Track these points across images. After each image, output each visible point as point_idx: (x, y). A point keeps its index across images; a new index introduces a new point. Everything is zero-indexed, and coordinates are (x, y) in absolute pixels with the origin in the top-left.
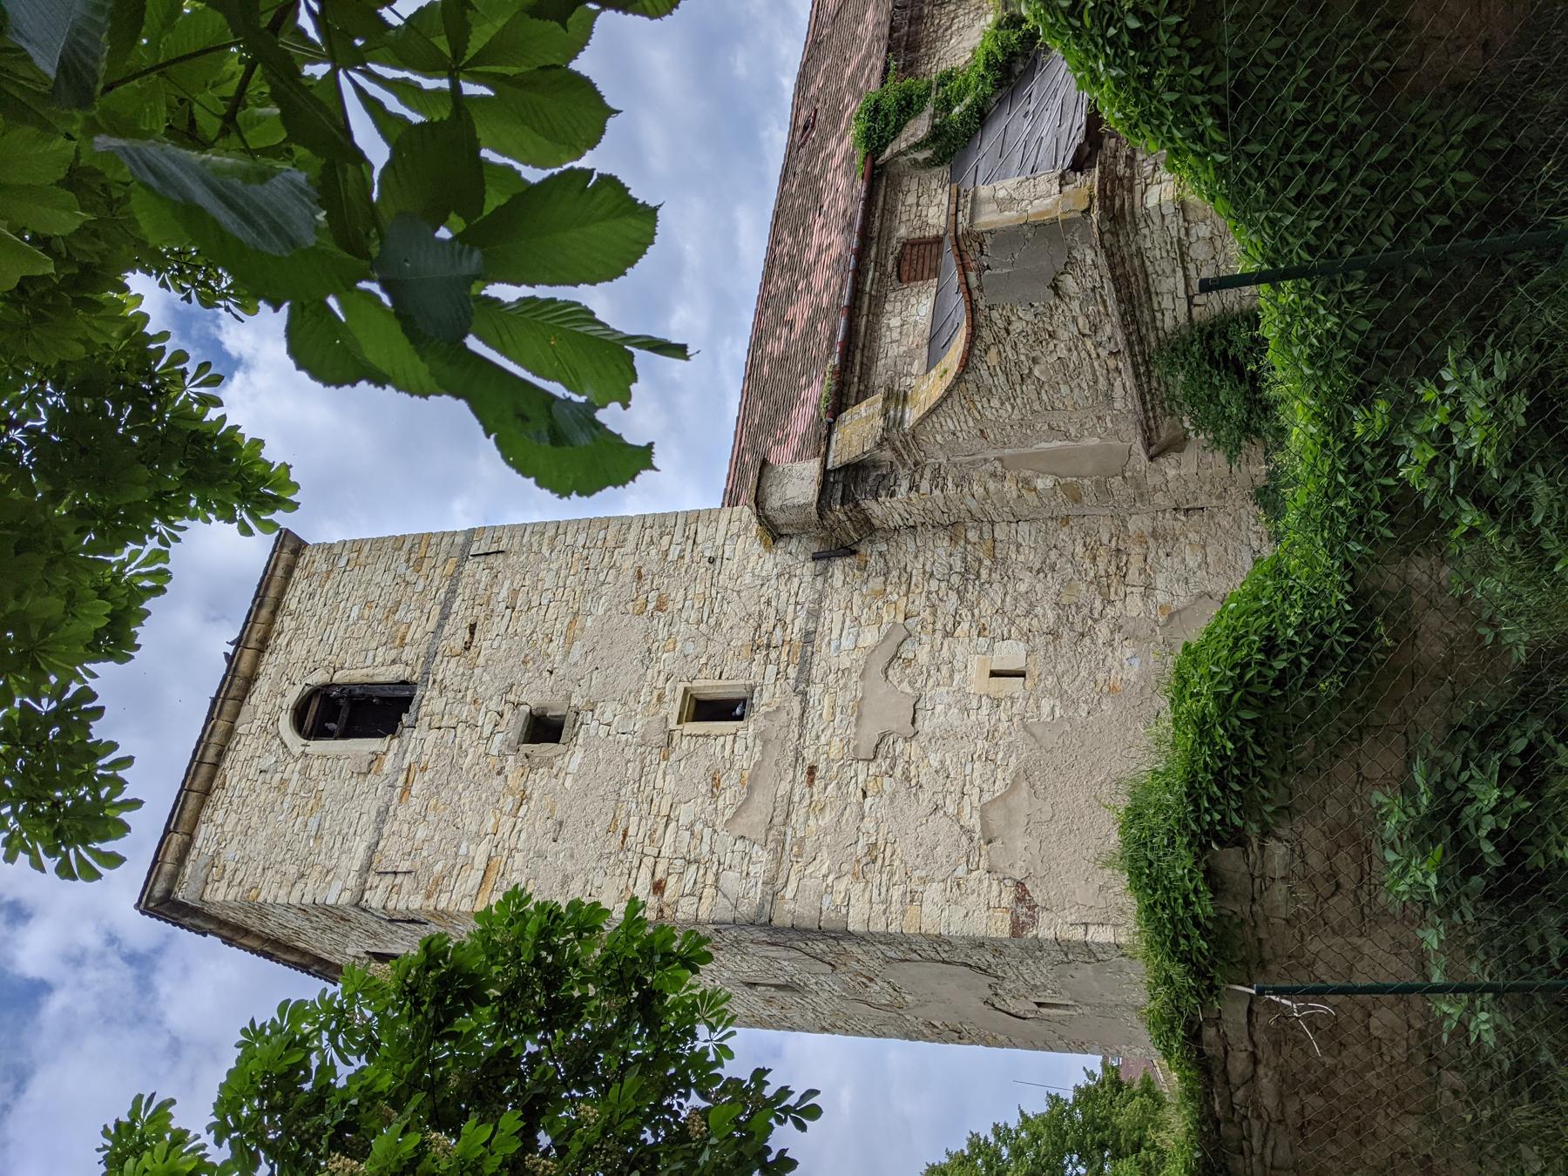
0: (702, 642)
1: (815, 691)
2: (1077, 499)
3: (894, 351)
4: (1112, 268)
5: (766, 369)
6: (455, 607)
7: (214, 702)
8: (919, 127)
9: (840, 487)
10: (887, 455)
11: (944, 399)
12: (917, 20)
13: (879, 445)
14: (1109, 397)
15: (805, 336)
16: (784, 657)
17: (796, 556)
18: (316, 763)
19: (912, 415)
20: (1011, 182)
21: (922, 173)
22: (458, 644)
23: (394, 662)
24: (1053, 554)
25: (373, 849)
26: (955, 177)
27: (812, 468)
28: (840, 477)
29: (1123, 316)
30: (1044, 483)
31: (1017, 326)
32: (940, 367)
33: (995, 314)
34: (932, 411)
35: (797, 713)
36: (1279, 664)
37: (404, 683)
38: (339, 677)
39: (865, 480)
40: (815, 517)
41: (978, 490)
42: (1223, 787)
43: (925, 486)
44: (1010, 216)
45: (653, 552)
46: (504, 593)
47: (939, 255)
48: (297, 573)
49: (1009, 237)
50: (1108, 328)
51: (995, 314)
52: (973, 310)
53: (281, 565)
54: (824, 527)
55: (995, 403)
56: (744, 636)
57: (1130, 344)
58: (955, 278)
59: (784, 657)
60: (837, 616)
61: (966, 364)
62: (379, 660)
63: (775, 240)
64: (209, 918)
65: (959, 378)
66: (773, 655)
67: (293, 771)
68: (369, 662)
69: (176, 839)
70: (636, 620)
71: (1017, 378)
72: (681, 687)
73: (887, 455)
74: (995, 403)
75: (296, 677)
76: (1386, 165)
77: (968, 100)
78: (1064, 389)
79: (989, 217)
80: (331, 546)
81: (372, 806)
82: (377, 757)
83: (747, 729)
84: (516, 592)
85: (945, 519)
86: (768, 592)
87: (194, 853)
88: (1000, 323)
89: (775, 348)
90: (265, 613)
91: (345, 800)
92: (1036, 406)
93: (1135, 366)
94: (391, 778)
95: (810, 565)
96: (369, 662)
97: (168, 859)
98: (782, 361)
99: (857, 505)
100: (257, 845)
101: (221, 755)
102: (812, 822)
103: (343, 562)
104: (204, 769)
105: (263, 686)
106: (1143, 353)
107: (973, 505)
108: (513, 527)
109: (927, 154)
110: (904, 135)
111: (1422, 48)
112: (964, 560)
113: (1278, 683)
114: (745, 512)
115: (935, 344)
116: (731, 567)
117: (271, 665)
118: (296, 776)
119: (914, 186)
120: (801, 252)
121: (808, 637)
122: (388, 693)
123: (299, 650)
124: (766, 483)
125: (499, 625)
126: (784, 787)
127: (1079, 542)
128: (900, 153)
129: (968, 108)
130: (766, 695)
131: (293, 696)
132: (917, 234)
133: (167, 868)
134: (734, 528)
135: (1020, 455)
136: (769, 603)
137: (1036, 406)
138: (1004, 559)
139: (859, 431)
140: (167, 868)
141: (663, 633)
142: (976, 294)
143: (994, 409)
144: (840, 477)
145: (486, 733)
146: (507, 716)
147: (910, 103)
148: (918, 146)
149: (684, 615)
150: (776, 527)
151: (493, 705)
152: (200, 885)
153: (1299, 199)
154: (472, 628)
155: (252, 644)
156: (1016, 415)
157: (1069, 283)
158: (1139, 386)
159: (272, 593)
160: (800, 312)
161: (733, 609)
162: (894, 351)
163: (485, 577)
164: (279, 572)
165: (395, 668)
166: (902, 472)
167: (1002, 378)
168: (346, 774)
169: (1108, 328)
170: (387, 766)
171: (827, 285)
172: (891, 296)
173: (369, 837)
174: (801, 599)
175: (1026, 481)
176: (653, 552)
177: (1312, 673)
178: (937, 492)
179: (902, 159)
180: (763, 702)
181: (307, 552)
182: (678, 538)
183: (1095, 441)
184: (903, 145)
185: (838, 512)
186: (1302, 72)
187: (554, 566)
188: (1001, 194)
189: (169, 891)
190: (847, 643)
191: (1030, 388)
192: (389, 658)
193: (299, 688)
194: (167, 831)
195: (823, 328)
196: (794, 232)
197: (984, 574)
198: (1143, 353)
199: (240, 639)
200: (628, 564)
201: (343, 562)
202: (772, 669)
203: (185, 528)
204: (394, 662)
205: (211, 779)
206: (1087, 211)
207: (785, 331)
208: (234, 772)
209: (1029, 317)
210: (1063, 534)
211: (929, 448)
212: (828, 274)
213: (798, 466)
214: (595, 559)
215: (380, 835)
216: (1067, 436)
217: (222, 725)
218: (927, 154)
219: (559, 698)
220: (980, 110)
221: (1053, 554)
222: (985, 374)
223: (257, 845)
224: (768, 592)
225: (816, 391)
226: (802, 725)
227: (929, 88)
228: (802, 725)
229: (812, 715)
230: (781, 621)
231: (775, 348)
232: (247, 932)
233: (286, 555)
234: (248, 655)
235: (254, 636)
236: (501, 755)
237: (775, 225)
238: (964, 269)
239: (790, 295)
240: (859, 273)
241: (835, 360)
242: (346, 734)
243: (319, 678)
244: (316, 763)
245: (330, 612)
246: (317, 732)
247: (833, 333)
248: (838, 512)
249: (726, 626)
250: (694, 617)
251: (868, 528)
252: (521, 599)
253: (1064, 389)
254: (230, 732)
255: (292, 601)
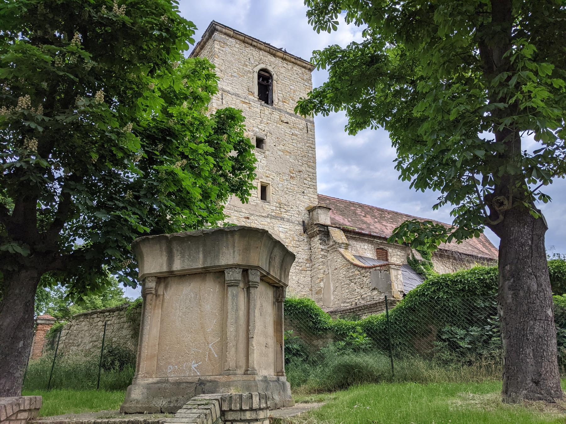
0: (282, 189)
1: (268, 220)
2: (317, 293)
3: (358, 246)
4: (379, 303)
5: (353, 208)
6: (293, 118)
7: (269, 45)
8: (418, 257)
9: (323, 230)
10: (331, 243)
11: (346, 259)
12: (448, 257)
13: (334, 241)
14: (344, 302)
15: (362, 221)
16: (277, 212)
17: (305, 217)
18: (251, 75)
19: (342, 250)
20: (402, 279)
21: (406, 257)
22: (283, 119)
23: (278, 99)
24: (302, 286)
25: (228, 92)
26: (404, 266)
27: (328, 222)
28: (326, 230)
29: (367, 306)
30: (322, 284)
31: (365, 279)
32: (354, 259)
33: (368, 273)
34: (343, 256)
35: (263, 215)
36: (314, 316)
37: (273, 102)
38: (274, 82)
39: (324, 237)
40: (315, 223)
41: (321, 267)
42: (289, 306)
43: (322, 253)
44: (393, 278)
45: (306, 176)
46: (296, 132)
47: (383, 260)
48: (304, 69)
49: (388, 277)
50: (363, 302)
51: (368, 273)
52: (370, 268)
53: (306, 65)
54: (311, 225)
55: (344, 273)
56: (283, 201)
57: (359, 307)
58: (377, 263)
59: (277, 212)
60: (288, 227)
61: (355, 265)
62: (279, 95)
63: (389, 212)
64: (207, 40)
65: (352, 263)
66: (278, 209)
67: (249, 68)
68: (279, 92)
69: (232, 33)
70: (288, 170)
71: (351, 278)
72: (270, 182)
73: (331, 243)
74: (344, 273)
75: (275, 69)
76: (401, 331)
77: (424, 270)
78: (347, 291)
79: (393, 273)
80: (311, 80)
81: (240, 92)
82: (253, 94)
83: (259, 201)
84: (297, 136)
85: (312, 258)
86: (295, 208)
87: (227, 38)
88: (366, 275)
89: (359, 211)
90: (293, 60)
91: (241, 84)
92: (343, 283)
93: (353, 309)
94: (247, 98)
95: (302, 220)
96: (279, 92)
97: (226, 30)
98: (355, 213)
99: (318, 234)
100: (229, 58)
101: (254, 46)
102: (235, 218)
103: (306, 84)
104: (250, 42)
105: (273, 59)
106: (356, 311)
107: (316, 266)
108: (314, 135)
109: (411, 258)
110: (416, 252)
111: (419, 340)
112: (302, 262)
113: (310, 316)
114: (316, 203)
115: (360, 257)
116: (302, 198)
117: (278, 61)
118: (248, 69)
119: (402, 254)
120: (385, 220)
121: (282, 219)
122: (270, 97)
123: (282, 70)
124: (325, 209)
125: (288, 131)
126: (244, 210)
127: (305, 293)
128: (411, 251)
129: (423, 270)
130: (267, 206)
131: (270, 68)
132: (389, 254)
133: (224, 30)
134: (312, 199)
135: (329, 279)
136: (292, 208)
137: (343, 283)
138: (301, 273)
139: (338, 236)
140: (224, 30)
141: (284, 178)
142: (374, 269)
143: (343, 272)
144: (326, 230)
145: (260, 127)
146: (263, 133)
147: (425, 254)
148: (413, 256)
149: (289, 184)
150: (312, 211)
151: (266, 128)
152: (219, 40)
153: (396, 319)
154: (287, 123)
155: (284, 56)
156: (340, 278)
157: (375, 292)
158: (347, 310)
159: (299, 62)
160: (369, 219)
161: (290, 198)
162: (358, 246)
163: (301, 127)
164: (304, 65)
165: (277, 100)
166: (326, 247)
167: (351, 275)
168: (248, 84)
169: (363, 302)
170: (251, 97)
171: (376, 228)
172: (373, 246)
173: (232, 91)
174: (293, 217)
175: (323, 280)
176: (306, 176)
177: (313, 322)
178: (321, 256)
179: (410, 251)
180: (266, 205)
181: (309, 73)
182: (310, 183)
183: (332, 298)
184: (414, 252)
185: (316, 229)
186: (416, 319)
187: (303, 147)
188: (399, 276)
189: (217, 30)
190: (281, 229)
191: (348, 282)
192: (279, 98)
193: (272, 70)
194: (234, 30)
195: (364, 226)
196: (391, 218)
197: (298, 268)
198: (356, 311)
199: (286, 53)
200: (303, 168)
201: (306, 84)
202: (274, 208)
203: (312, 25)
204: (278, 99)
205: (248, 43)
206: (393, 297)
207: (363, 215)
208: (250, 50)
209: (367, 282)
210: (307, 289)
211: (333, 254)
212: (379, 228)
213: (329, 218)
214: (305, 159)
215: (232, 95)
216: (334, 291)
217: (263, 47)
218: (411, 258)
219: (268, 148)
220: (422, 273)
221: (302, 286)
222: (353, 270)
223: (229, 58)
224: (295, 208)
225: (347, 223)
226: (260, 216)
227: (429, 260)
228: (260, 216)
229: (262, 219)
230: (287, 211)
231: (359, 211)
232: (201, 49)
233: (309, 66)
234: (281, 55)
235: (287, 57)
236: (253, 131)
237: (393, 212)
238: (381, 266)
239: (374, 216)
240: (380, 238)
241: (357, 230)
242: (259, 83)
243: (275, 77)
244: (251, 75)
245: (292, 80)
246: (260, 76)
247: (363, 229)
248: (316, 229)
249: (286, 196)
250: (288, 187)
251: (311, 237)
252: (295, 137)
253: (347, 291)
254: (260, 49)
255: (296, 68)
